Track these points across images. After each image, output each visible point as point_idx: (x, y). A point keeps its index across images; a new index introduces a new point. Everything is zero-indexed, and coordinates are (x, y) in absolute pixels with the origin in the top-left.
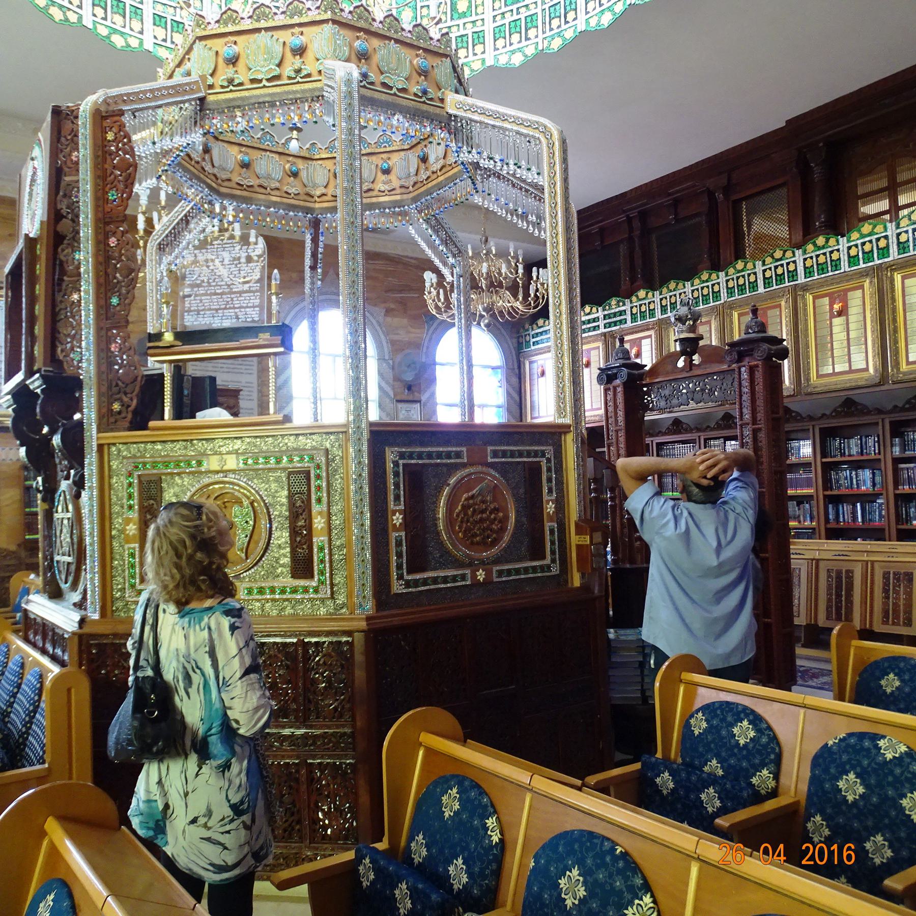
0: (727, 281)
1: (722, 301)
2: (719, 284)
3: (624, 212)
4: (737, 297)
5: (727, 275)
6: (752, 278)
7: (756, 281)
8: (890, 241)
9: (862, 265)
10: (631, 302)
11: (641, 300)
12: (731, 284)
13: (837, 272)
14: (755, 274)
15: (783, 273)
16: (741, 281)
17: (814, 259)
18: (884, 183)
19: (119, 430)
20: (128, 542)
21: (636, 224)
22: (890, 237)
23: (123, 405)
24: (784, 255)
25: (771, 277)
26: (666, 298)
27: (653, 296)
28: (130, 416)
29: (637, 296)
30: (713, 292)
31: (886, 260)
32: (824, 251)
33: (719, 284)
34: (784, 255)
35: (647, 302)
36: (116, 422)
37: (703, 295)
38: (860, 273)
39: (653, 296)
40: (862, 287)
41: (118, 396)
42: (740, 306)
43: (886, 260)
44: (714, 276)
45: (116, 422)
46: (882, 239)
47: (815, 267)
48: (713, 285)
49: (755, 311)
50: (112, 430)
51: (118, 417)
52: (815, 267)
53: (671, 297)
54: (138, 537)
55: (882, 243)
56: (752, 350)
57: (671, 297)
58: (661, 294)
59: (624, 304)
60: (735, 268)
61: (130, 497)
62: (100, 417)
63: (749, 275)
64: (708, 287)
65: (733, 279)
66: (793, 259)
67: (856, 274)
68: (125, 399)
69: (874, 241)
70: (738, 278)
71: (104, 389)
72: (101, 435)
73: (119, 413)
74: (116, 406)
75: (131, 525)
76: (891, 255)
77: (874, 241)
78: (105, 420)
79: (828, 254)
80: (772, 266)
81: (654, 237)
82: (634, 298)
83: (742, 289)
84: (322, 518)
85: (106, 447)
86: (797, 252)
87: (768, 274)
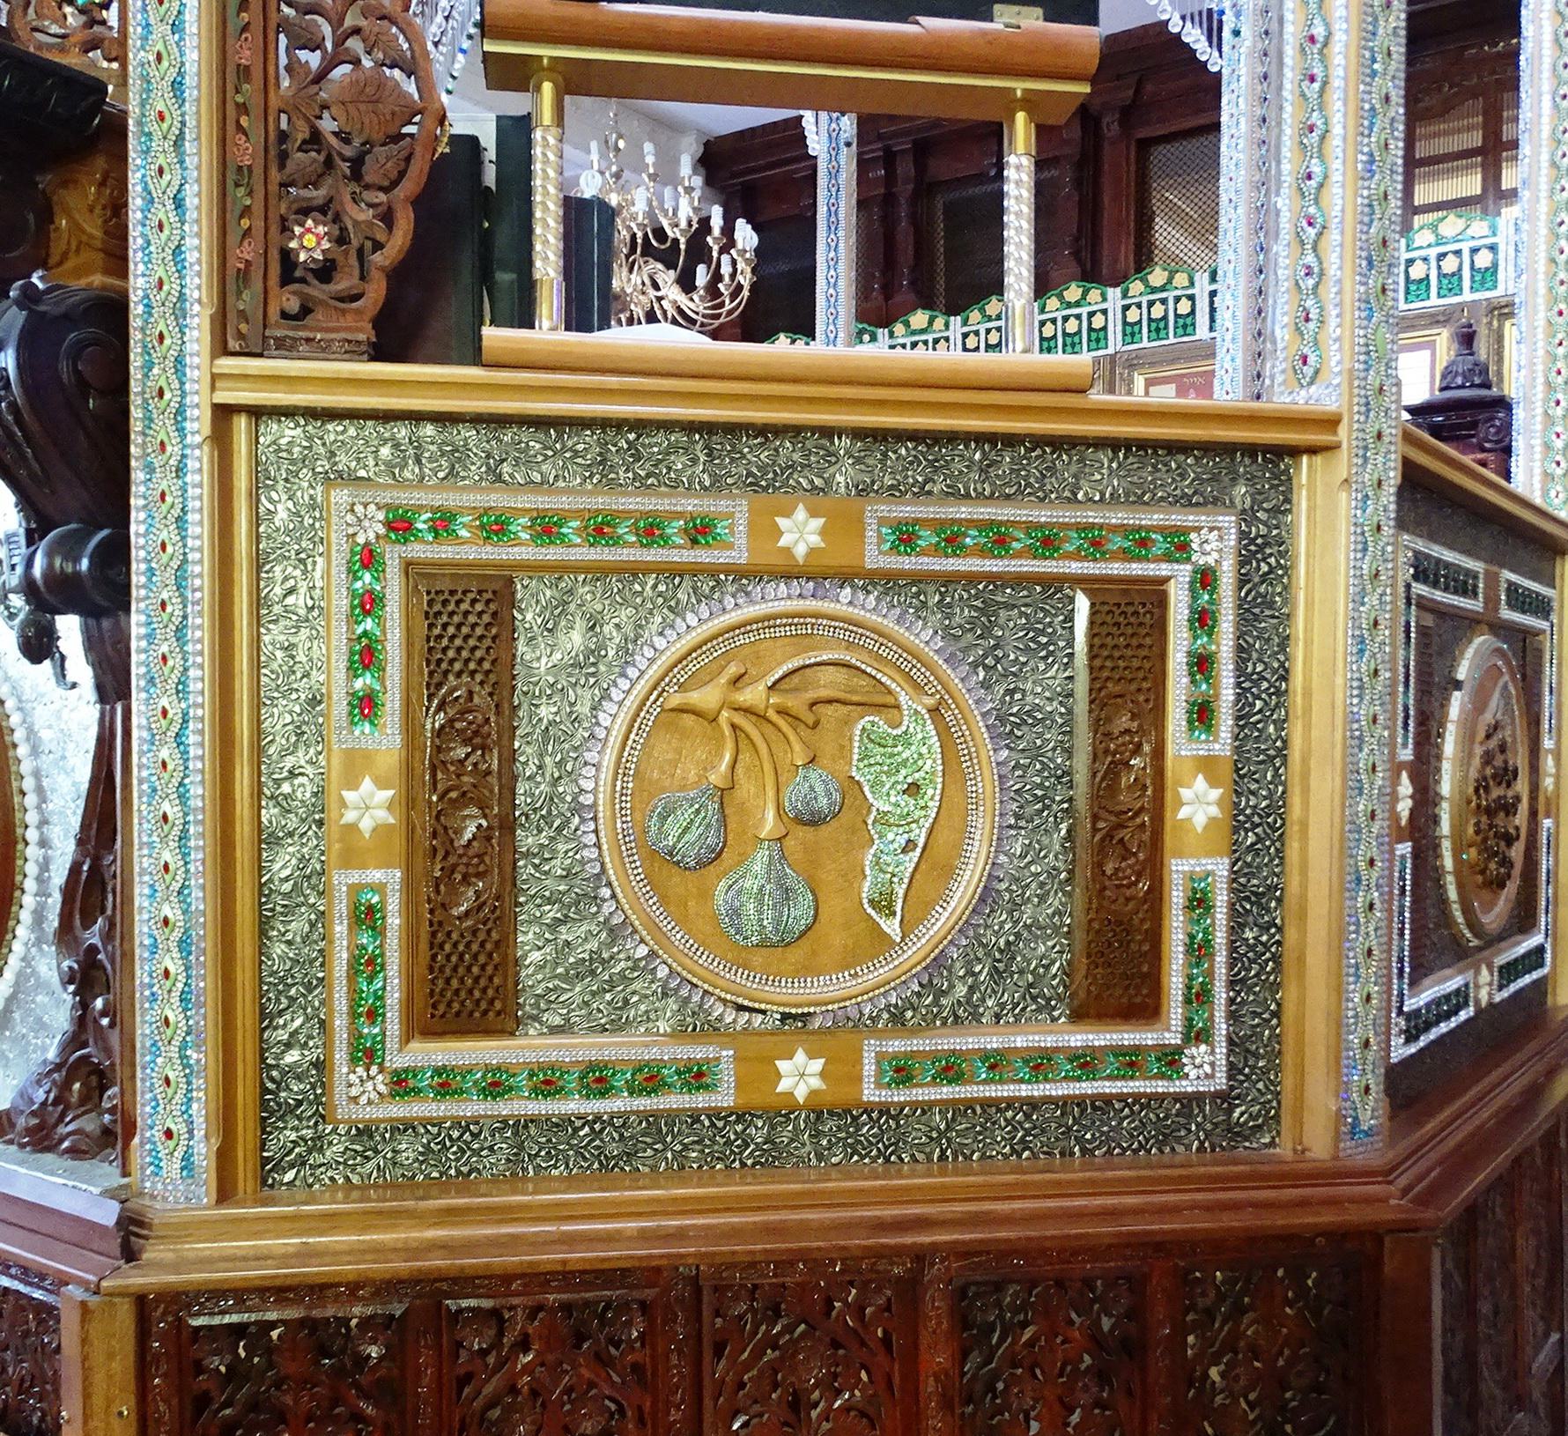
0: (1126, 308)
1: (1110, 351)
2: (1105, 312)
3: (880, 137)
4: (1146, 343)
5: (1125, 295)
6: (1184, 307)
7: (1193, 312)
8: (1501, 256)
9: (1434, 301)
10: (891, 335)
11: (914, 333)
12: (1133, 315)
13: (1185, 339)
14: (1191, 298)
15: (1079, 332)
16: (1157, 312)
17: (1059, 323)
18: (1475, 139)
19: (323, 351)
20: (350, 859)
21: (905, 168)
22: (1502, 248)
23: (341, 240)
24: (1170, 281)
25: (1055, 336)
26: (977, 333)
27: (947, 326)
28: (376, 291)
29: (907, 324)
30: (1090, 329)
31: (1488, 294)
32: (1164, 295)
33: (1105, 312)
34: (1170, 281)
35: (930, 337)
36: (305, 311)
37: (1065, 334)
38: (1432, 315)
39: (947, 326)
40: (1431, 346)
41: (318, 195)
42: (1152, 364)
43: (1488, 294)
44: (1094, 295)
45: (305, 311)
46: (1450, 256)
47: (1145, 323)
48: (1091, 314)
49: (1467, 339)
50: (285, 347)
51: (317, 290)
52: (1145, 323)
53: (988, 331)
54: (398, 843)
55: (1483, 260)
56: (1474, 425)
57: (988, 331)
58: (965, 323)
59: (873, 338)
60: (1060, 297)
61: (366, 656)
62: (228, 280)
63: (1177, 299)
64: (1078, 317)
65: (1139, 306)
66: (1189, 292)
67: (1421, 316)
68: (359, 214)
69: (1144, 305)
70: (1151, 304)
71: (247, 152)
72: (228, 364)
73: (325, 271)
74: (311, 242)
75: (367, 784)
76: (1111, 343)
77: (1144, 305)
78: (248, 300)
79: (1059, 323)
80: (1144, 300)
81: (939, 204)
82: (899, 328)
83: (1158, 327)
84: (1213, 782)
85: (241, 423)
86: (1110, 291)
87: (1133, 315)
